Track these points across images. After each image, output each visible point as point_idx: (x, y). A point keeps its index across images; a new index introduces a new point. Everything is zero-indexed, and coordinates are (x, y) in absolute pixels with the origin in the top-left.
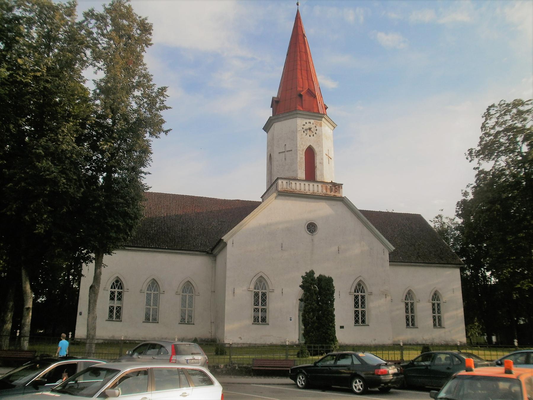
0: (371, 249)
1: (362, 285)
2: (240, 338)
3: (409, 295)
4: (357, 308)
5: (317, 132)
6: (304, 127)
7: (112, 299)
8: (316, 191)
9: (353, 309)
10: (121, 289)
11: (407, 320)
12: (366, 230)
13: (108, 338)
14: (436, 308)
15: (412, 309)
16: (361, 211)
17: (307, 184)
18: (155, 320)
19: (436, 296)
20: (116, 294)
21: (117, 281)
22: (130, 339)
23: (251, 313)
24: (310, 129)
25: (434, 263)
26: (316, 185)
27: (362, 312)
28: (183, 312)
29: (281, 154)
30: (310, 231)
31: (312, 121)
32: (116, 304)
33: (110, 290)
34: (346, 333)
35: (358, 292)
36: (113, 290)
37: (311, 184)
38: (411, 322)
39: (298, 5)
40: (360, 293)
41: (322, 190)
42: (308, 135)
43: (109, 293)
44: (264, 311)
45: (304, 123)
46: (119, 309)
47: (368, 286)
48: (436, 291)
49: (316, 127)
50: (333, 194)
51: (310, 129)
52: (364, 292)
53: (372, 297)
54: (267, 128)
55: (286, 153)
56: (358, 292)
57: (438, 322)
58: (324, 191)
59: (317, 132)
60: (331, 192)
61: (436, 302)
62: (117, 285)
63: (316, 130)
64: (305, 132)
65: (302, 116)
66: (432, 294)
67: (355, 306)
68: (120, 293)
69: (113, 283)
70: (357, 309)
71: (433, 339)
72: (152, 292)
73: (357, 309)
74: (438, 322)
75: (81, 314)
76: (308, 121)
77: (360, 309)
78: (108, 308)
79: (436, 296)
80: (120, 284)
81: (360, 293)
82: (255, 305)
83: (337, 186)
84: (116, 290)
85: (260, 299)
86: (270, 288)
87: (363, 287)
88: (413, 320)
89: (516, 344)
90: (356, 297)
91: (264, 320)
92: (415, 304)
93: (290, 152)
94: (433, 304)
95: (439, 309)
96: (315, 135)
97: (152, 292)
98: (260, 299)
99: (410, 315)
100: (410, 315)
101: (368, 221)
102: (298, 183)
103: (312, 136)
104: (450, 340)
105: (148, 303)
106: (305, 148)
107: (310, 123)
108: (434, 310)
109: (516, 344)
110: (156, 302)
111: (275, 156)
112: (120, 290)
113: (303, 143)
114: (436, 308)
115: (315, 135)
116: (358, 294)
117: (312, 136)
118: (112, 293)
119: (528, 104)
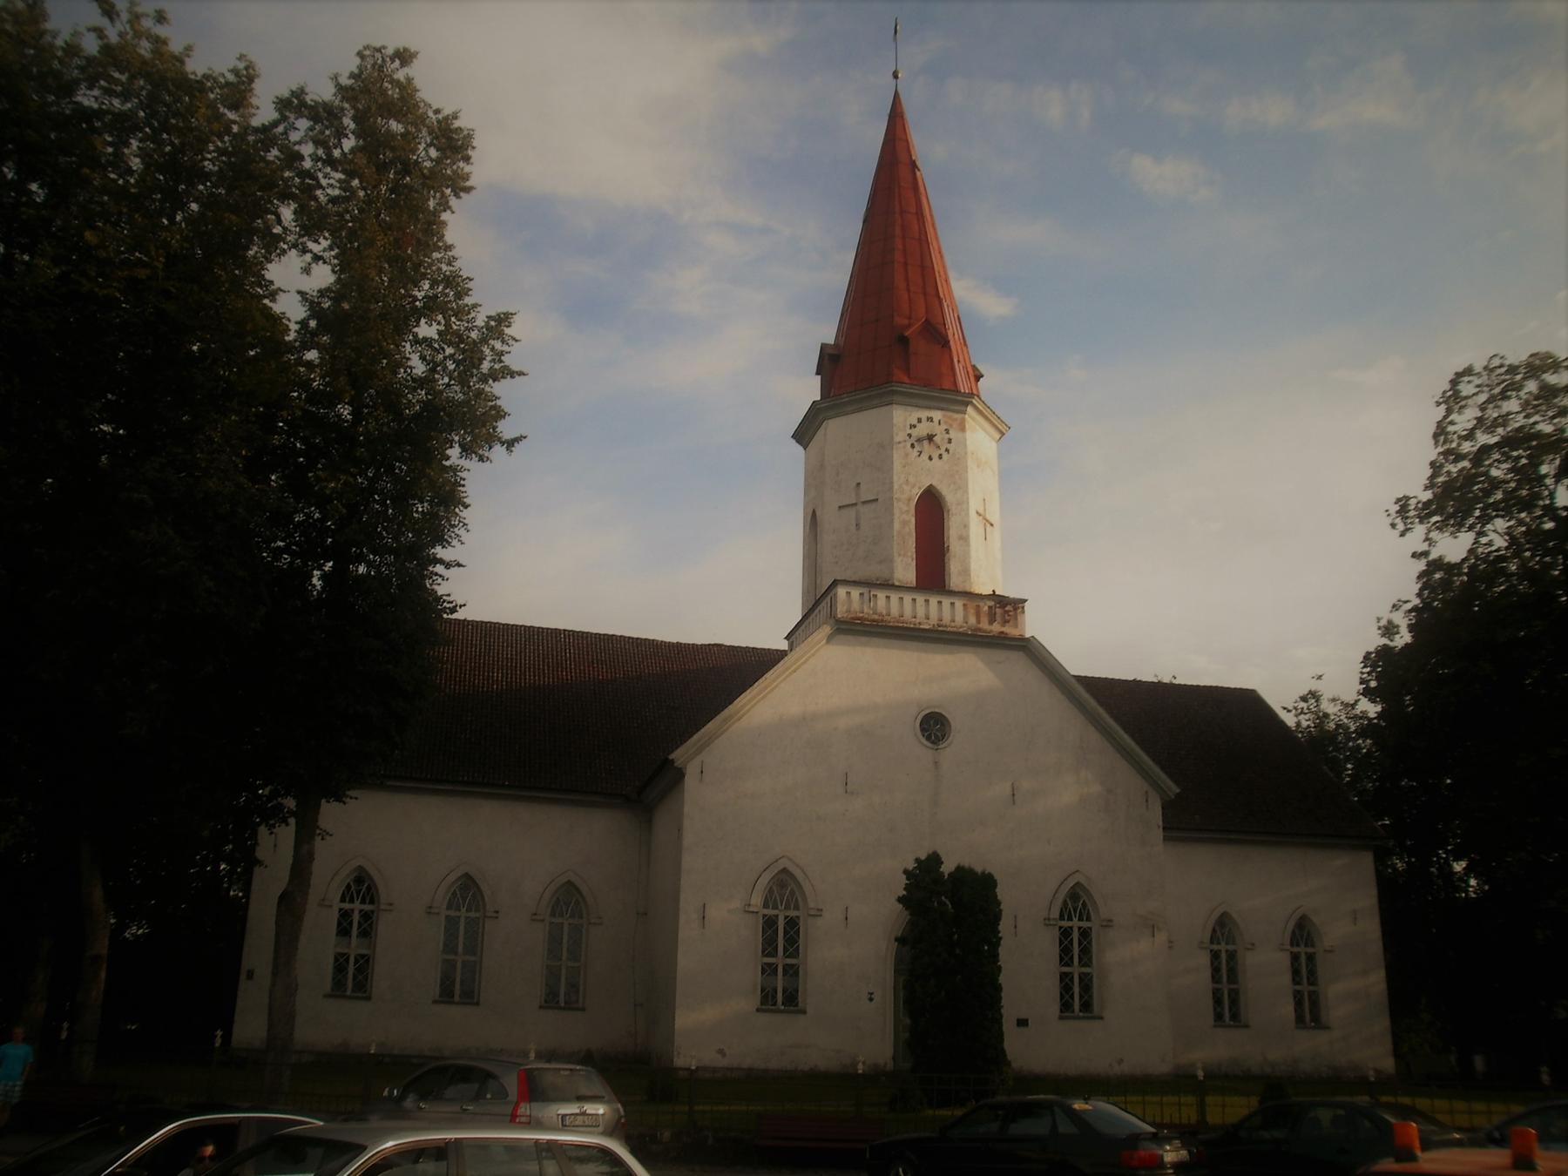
2: (721, 1052)
4: (1067, 965)
5: (951, 447)
7: (343, 931)
10: (372, 902)
11: (1218, 1001)
12: (1094, 737)
16: (1079, 679)
17: (920, 599)
18: (470, 997)
19: (1303, 932)
20: (356, 917)
21: (359, 880)
22: (396, 1052)
24: (930, 438)
26: (946, 602)
28: (1065, 981)
29: (844, 511)
31: (937, 415)
32: (355, 946)
33: (337, 905)
35: (1070, 919)
37: (934, 600)
39: (895, 76)
40: (1075, 920)
42: (925, 457)
44: (792, 972)
46: (364, 963)
49: (947, 431)
50: (996, 628)
51: (930, 438)
52: (1088, 919)
54: (803, 435)
55: (863, 509)
56: (1070, 919)
57: (1309, 1012)
58: (972, 620)
59: (951, 447)
61: (1223, 947)
62: (358, 893)
63: (950, 441)
64: (918, 447)
67: (1061, 959)
68: (366, 916)
69: (348, 887)
70: (1066, 969)
72: (1075, 923)
73: (1066, 969)
74: (1309, 1012)
75: (250, 975)
76: (924, 414)
78: (331, 960)
80: (369, 888)
81: (1075, 920)
82: (765, 953)
83: (1008, 607)
84: (357, 905)
86: (812, 905)
88: (1234, 1002)
89: (1545, 1078)
90: (1066, 933)
91: (791, 999)
93: (873, 506)
96: (945, 456)
97: (1075, 923)
100: (1076, 970)
102: (894, 597)
103: (935, 457)
105: (449, 947)
106: (917, 492)
107: (930, 419)
109: (1545, 1078)
111: (829, 516)
112: (367, 907)
113: (911, 479)
117: (935, 457)
118: (345, 915)
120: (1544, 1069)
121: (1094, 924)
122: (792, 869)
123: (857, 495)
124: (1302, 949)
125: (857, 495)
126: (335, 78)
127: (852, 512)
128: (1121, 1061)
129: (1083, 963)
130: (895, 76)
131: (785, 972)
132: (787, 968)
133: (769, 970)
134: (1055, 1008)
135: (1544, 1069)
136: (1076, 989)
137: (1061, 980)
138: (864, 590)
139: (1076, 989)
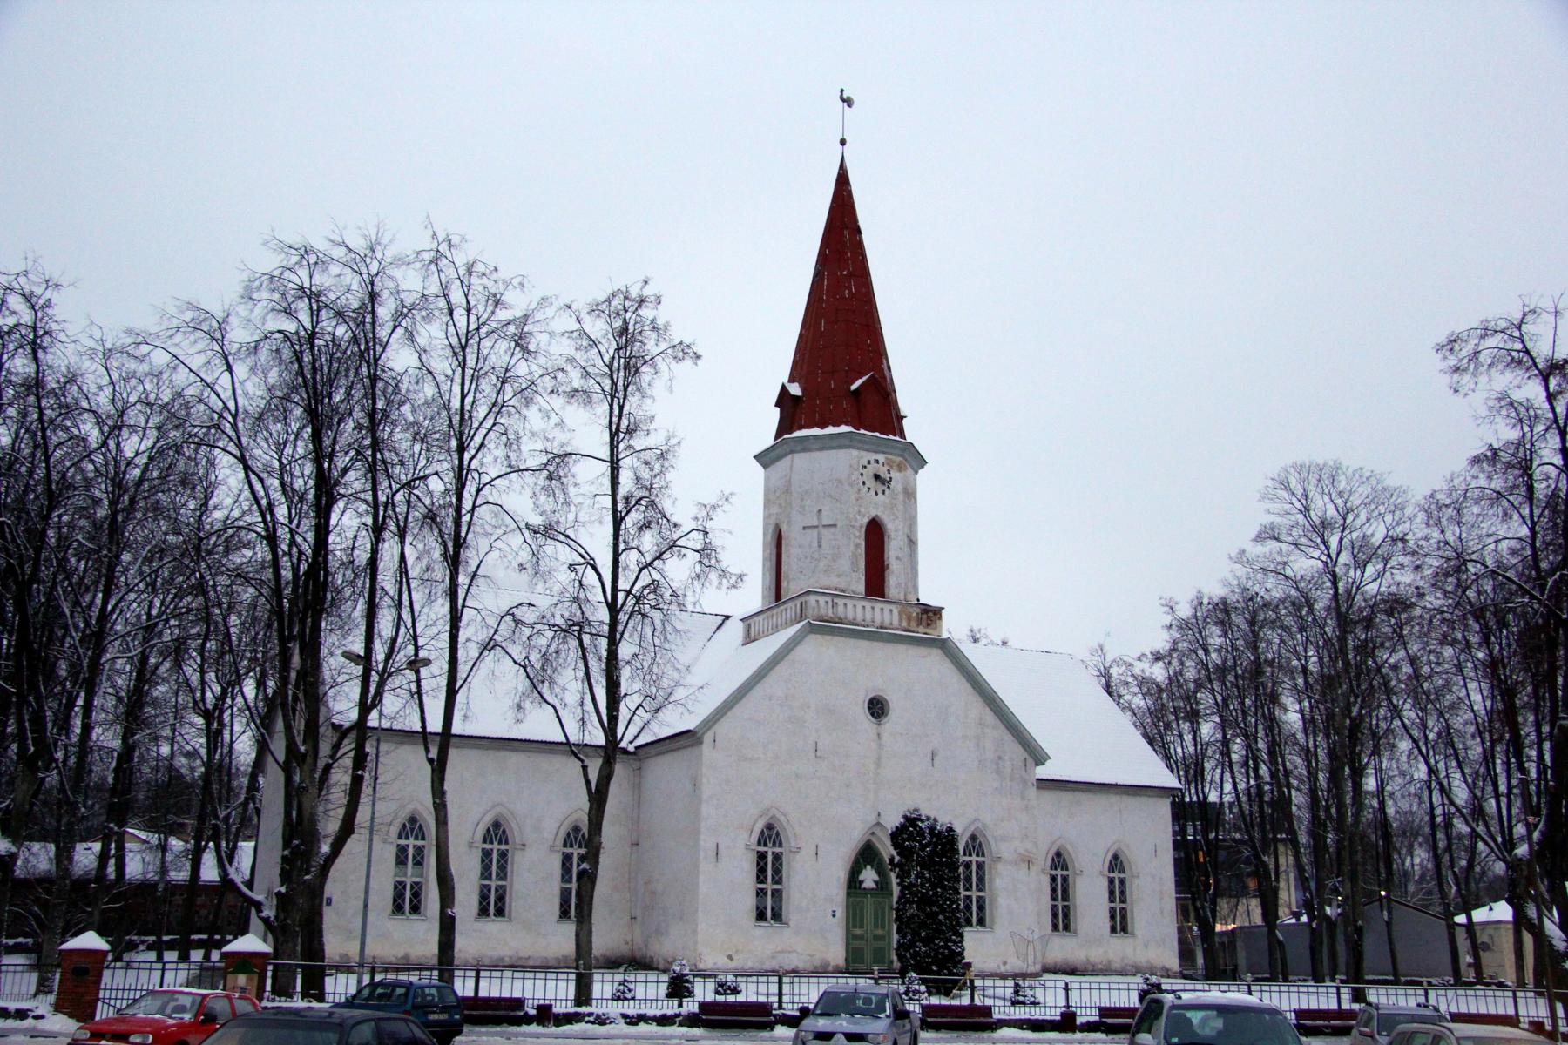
2: (730, 958)
3: (1059, 860)
4: (761, 882)
7: (401, 860)
9: (1127, 905)
11: (1055, 915)
13: (394, 960)
14: (1118, 891)
15: (1065, 891)
17: (868, 605)
19: (1116, 863)
20: (411, 851)
23: (749, 901)
26: (887, 607)
27: (979, 899)
29: (809, 531)
31: (881, 458)
36: (487, 846)
37: (878, 606)
38: (1062, 919)
39: (843, 142)
42: (872, 492)
43: (480, 854)
44: (777, 894)
47: (992, 842)
53: (1000, 866)
55: (825, 532)
61: (1059, 872)
66: (1109, 857)
72: (496, 846)
74: (1120, 923)
75: (329, 902)
76: (873, 457)
77: (494, 884)
78: (391, 888)
79: (1116, 863)
83: (931, 614)
84: (411, 842)
85: (769, 865)
88: (1066, 916)
90: (487, 854)
91: (777, 916)
92: (1128, 883)
94: (1111, 881)
95: (1122, 893)
98: (769, 865)
99: (1060, 904)
100: (1060, 904)
102: (850, 603)
106: (866, 520)
107: (877, 461)
108: (1111, 893)
110: (503, 873)
111: (792, 535)
112: (420, 843)
114: (1118, 891)
116: (967, 858)
118: (402, 851)
119: (271, 506)
122: (778, 815)
123: (819, 519)
125: (819, 519)
127: (815, 532)
128: (1005, 963)
129: (499, 878)
130: (843, 142)
133: (761, 893)
134: (1107, 924)
136: (974, 909)
137: (396, 887)
138: (829, 599)
139: (974, 909)
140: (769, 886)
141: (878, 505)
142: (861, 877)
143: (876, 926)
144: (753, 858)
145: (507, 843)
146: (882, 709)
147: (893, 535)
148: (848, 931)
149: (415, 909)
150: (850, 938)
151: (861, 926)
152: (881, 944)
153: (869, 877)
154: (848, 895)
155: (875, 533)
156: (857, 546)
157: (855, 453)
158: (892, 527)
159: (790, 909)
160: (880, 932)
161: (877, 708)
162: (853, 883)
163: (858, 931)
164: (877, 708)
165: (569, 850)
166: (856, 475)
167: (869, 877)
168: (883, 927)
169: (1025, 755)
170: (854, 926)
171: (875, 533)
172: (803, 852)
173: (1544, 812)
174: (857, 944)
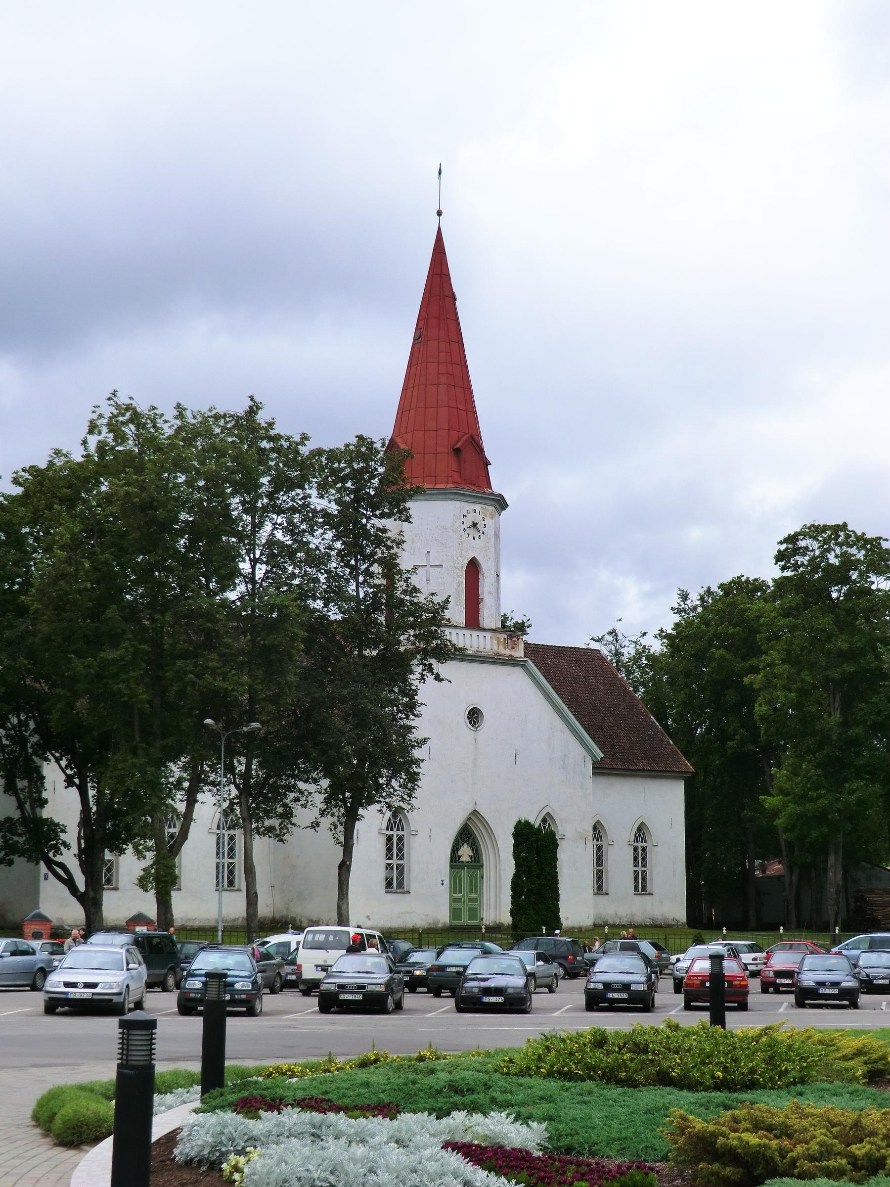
0: (565, 756)
1: (549, 821)
2: (368, 917)
4: (389, 859)
6: (465, 526)
8: (481, 649)
9: (647, 869)
12: (559, 723)
14: (640, 857)
17: (468, 632)
19: (641, 832)
21: (639, 829)
24: (475, 525)
25: (644, 770)
26: (482, 634)
30: (470, 723)
31: (478, 507)
34: (576, 906)
36: (389, 833)
39: (439, 213)
40: (395, 830)
41: (492, 644)
42: (471, 537)
44: (401, 869)
45: (466, 513)
48: (643, 824)
50: (508, 652)
51: (475, 525)
55: (432, 570)
56: (392, 830)
57: (641, 885)
58: (495, 648)
60: (505, 648)
65: (462, 498)
71: (633, 915)
74: (641, 885)
76: (471, 507)
79: (641, 832)
86: (412, 828)
87: (549, 825)
89: (544, 931)
90: (389, 839)
93: (439, 569)
95: (644, 859)
96: (482, 535)
101: (564, 705)
103: (477, 538)
104: (659, 917)
106: (466, 561)
107: (474, 511)
109: (544, 931)
113: (463, 553)
114: (640, 857)
115: (482, 535)
117: (477, 538)
120: (781, 928)
121: (647, 844)
123: (428, 560)
124: (639, 844)
125: (428, 560)
126: (305, 438)
130: (439, 213)
131: (397, 869)
132: (398, 866)
133: (389, 867)
135: (781, 928)
140: (395, 862)
141: (475, 548)
142: (460, 853)
143: (471, 892)
144: (383, 840)
145: (403, 830)
146: (477, 718)
147: (486, 574)
148: (451, 896)
149: (231, 883)
150: (453, 900)
151: (460, 892)
152: (473, 905)
153: (465, 853)
154: (451, 867)
155: (473, 569)
156: (460, 584)
157: (457, 504)
158: (486, 566)
159: (413, 880)
160: (473, 895)
161: (474, 716)
162: (454, 858)
163: (458, 895)
164: (474, 716)
165: (636, 844)
166: (459, 522)
167: (465, 853)
168: (476, 892)
169: (585, 753)
170: (455, 892)
171: (473, 569)
172: (420, 834)
173: (784, 853)
174: (458, 905)
